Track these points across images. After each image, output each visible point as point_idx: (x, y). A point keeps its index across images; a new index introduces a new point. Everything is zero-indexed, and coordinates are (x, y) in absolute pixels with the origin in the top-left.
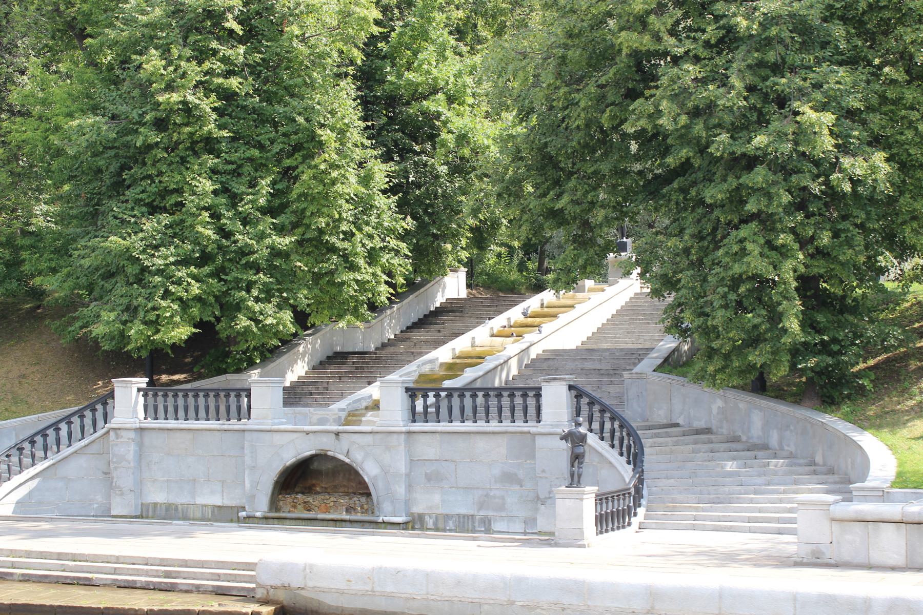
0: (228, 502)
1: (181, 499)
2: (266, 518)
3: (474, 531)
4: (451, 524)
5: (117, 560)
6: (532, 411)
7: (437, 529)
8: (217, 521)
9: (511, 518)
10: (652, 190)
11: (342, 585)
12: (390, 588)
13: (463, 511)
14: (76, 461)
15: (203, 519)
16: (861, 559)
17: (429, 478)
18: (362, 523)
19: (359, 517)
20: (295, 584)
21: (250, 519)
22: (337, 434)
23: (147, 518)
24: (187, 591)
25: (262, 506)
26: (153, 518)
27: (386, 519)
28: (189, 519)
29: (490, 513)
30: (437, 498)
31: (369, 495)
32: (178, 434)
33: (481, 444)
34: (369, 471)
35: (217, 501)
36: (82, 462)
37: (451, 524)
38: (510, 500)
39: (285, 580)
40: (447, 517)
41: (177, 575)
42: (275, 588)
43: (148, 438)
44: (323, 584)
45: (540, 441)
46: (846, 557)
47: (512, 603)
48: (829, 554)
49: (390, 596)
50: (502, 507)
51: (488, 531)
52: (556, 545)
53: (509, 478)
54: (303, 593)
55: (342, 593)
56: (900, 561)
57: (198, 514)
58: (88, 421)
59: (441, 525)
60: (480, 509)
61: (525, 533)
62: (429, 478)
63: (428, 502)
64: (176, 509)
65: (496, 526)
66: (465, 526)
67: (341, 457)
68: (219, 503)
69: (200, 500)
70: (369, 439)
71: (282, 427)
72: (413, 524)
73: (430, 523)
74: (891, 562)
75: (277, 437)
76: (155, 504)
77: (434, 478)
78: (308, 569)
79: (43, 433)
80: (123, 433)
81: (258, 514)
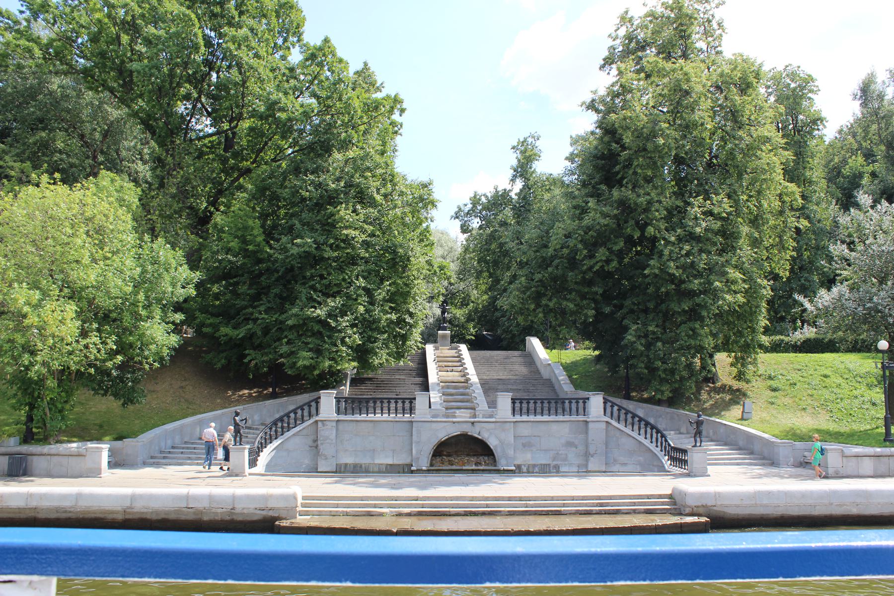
0: (396, 462)
1: (365, 461)
2: (428, 471)
3: (550, 472)
4: (537, 470)
5: (487, 499)
6: (581, 410)
7: (528, 472)
8: (389, 473)
9: (571, 465)
10: (54, 357)
11: (739, 503)
12: (765, 502)
13: (544, 462)
14: (295, 438)
15: (379, 472)
16: (856, 473)
17: (524, 445)
18: (490, 471)
19: (454, 467)
20: (709, 504)
21: (419, 471)
22: (473, 423)
23: (340, 472)
24: (626, 513)
25: (425, 464)
26: (344, 472)
27: (506, 468)
28: (369, 472)
29: (559, 463)
30: (529, 455)
31: (493, 454)
32: (363, 424)
33: (554, 427)
34: (492, 443)
35: (390, 461)
36: (297, 440)
37: (537, 470)
38: (571, 456)
39: (704, 502)
40: (534, 466)
41: (607, 505)
42: (698, 507)
43: (341, 426)
44: (726, 502)
45: (591, 425)
46: (849, 473)
47: (832, 504)
48: (842, 472)
49: (766, 506)
50: (566, 459)
51: (558, 472)
52: (695, 476)
53: (570, 444)
54: (715, 508)
55: (737, 506)
56: (871, 473)
57: (376, 469)
58: (306, 413)
59: (531, 470)
60: (553, 461)
61: (578, 472)
62: (524, 445)
63: (525, 458)
64: (361, 466)
65: (562, 469)
66: (544, 470)
67: (476, 436)
68: (391, 463)
69: (377, 461)
70: (492, 425)
71: (439, 419)
72: (518, 471)
73: (525, 469)
74: (868, 474)
75: (434, 425)
76: (346, 465)
77: (527, 446)
78: (717, 495)
79: (281, 419)
80: (327, 423)
81: (424, 468)
